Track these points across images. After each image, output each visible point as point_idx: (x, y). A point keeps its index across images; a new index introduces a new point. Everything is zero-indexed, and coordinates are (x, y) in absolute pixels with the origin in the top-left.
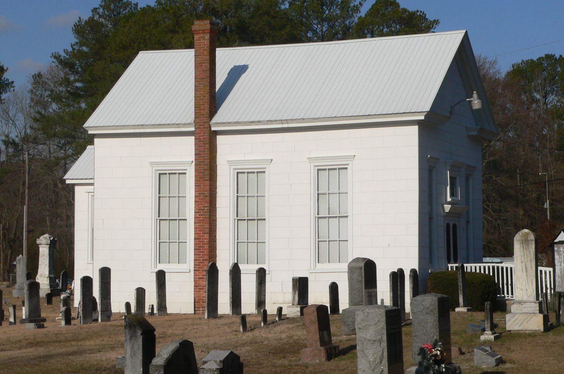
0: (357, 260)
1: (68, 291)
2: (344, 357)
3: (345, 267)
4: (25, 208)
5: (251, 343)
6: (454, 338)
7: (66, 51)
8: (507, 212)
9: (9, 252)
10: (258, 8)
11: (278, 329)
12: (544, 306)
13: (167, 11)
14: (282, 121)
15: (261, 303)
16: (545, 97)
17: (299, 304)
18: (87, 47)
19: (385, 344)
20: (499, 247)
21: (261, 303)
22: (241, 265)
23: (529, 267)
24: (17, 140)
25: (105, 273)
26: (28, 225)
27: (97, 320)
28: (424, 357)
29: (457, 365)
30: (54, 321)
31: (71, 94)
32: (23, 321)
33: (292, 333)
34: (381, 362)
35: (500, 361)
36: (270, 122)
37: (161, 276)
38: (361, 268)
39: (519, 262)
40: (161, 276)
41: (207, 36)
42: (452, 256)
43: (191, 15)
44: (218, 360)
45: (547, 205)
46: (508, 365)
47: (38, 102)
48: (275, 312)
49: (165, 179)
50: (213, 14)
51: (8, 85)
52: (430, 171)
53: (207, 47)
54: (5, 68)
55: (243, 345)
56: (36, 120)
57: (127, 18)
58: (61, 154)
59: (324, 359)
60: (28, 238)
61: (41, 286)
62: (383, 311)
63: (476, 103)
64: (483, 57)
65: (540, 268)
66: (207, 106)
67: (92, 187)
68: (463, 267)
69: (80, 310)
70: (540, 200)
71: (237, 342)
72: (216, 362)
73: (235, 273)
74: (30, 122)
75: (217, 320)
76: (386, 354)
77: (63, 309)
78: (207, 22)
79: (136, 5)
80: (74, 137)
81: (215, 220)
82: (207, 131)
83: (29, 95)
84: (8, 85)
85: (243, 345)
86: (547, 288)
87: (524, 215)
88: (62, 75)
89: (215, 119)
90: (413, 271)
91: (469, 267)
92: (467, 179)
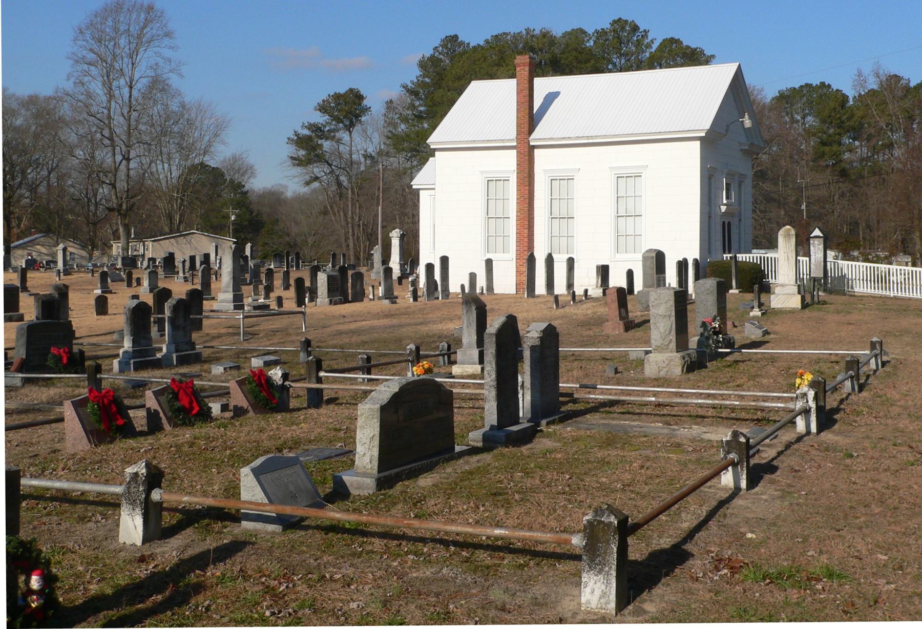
0: (650, 251)
1: (415, 275)
2: (639, 329)
3: (639, 257)
4: (380, 208)
5: (563, 317)
6: (729, 314)
7: (412, 82)
8: (771, 212)
9: (367, 244)
10: (567, 45)
11: (585, 306)
12: (802, 288)
13: (494, 48)
14: (588, 137)
15: (570, 285)
16: (803, 118)
17: (601, 286)
18: (429, 78)
19: (673, 319)
20: (764, 241)
21: (570, 285)
22: (78, 294)
23: (790, 257)
24: (373, 154)
25: (444, 261)
26: (382, 221)
27: (438, 298)
28: (705, 329)
29: (731, 336)
30: (404, 298)
31: (416, 116)
32: (380, 298)
33: (596, 310)
34: (670, 333)
35: (766, 333)
36: (578, 138)
37: (489, 263)
38: (653, 257)
39: (782, 253)
40: (489, 263)
41: (527, 69)
42: (727, 248)
43: (513, 51)
44: (539, 330)
45: (804, 207)
46: (772, 336)
47: (391, 124)
48: (582, 293)
49: (492, 184)
50: (531, 51)
51: (366, 109)
52: (710, 178)
53: (527, 78)
54: (364, 96)
55: (557, 319)
56: (388, 138)
57: (462, 54)
58: (408, 165)
59: (622, 331)
60: (382, 233)
61: (394, 271)
62: (672, 292)
63: (748, 123)
64: (752, 85)
65: (799, 258)
66: (527, 125)
67: (433, 191)
68: (735, 256)
69: (425, 290)
70: (798, 203)
71: (551, 317)
72: (537, 331)
73: (550, 261)
74: (383, 139)
75: (535, 299)
76: (674, 326)
77: (411, 289)
78: (527, 57)
79: (468, 44)
80: (418, 151)
81: (533, 218)
82: (527, 145)
83: (383, 118)
84: (366, 109)
85: (557, 319)
86: (803, 274)
87: (785, 214)
88: (409, 101)
89: (533, 136)
90: (696, 261)
91: (741, 257)
92: (740, 186)
